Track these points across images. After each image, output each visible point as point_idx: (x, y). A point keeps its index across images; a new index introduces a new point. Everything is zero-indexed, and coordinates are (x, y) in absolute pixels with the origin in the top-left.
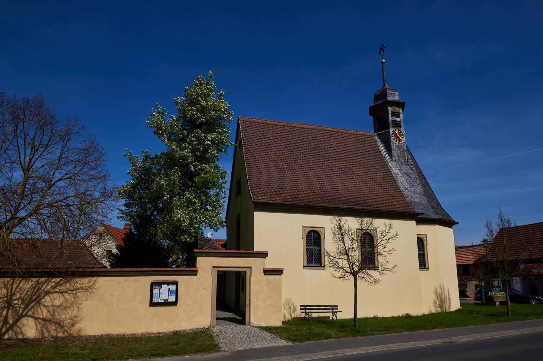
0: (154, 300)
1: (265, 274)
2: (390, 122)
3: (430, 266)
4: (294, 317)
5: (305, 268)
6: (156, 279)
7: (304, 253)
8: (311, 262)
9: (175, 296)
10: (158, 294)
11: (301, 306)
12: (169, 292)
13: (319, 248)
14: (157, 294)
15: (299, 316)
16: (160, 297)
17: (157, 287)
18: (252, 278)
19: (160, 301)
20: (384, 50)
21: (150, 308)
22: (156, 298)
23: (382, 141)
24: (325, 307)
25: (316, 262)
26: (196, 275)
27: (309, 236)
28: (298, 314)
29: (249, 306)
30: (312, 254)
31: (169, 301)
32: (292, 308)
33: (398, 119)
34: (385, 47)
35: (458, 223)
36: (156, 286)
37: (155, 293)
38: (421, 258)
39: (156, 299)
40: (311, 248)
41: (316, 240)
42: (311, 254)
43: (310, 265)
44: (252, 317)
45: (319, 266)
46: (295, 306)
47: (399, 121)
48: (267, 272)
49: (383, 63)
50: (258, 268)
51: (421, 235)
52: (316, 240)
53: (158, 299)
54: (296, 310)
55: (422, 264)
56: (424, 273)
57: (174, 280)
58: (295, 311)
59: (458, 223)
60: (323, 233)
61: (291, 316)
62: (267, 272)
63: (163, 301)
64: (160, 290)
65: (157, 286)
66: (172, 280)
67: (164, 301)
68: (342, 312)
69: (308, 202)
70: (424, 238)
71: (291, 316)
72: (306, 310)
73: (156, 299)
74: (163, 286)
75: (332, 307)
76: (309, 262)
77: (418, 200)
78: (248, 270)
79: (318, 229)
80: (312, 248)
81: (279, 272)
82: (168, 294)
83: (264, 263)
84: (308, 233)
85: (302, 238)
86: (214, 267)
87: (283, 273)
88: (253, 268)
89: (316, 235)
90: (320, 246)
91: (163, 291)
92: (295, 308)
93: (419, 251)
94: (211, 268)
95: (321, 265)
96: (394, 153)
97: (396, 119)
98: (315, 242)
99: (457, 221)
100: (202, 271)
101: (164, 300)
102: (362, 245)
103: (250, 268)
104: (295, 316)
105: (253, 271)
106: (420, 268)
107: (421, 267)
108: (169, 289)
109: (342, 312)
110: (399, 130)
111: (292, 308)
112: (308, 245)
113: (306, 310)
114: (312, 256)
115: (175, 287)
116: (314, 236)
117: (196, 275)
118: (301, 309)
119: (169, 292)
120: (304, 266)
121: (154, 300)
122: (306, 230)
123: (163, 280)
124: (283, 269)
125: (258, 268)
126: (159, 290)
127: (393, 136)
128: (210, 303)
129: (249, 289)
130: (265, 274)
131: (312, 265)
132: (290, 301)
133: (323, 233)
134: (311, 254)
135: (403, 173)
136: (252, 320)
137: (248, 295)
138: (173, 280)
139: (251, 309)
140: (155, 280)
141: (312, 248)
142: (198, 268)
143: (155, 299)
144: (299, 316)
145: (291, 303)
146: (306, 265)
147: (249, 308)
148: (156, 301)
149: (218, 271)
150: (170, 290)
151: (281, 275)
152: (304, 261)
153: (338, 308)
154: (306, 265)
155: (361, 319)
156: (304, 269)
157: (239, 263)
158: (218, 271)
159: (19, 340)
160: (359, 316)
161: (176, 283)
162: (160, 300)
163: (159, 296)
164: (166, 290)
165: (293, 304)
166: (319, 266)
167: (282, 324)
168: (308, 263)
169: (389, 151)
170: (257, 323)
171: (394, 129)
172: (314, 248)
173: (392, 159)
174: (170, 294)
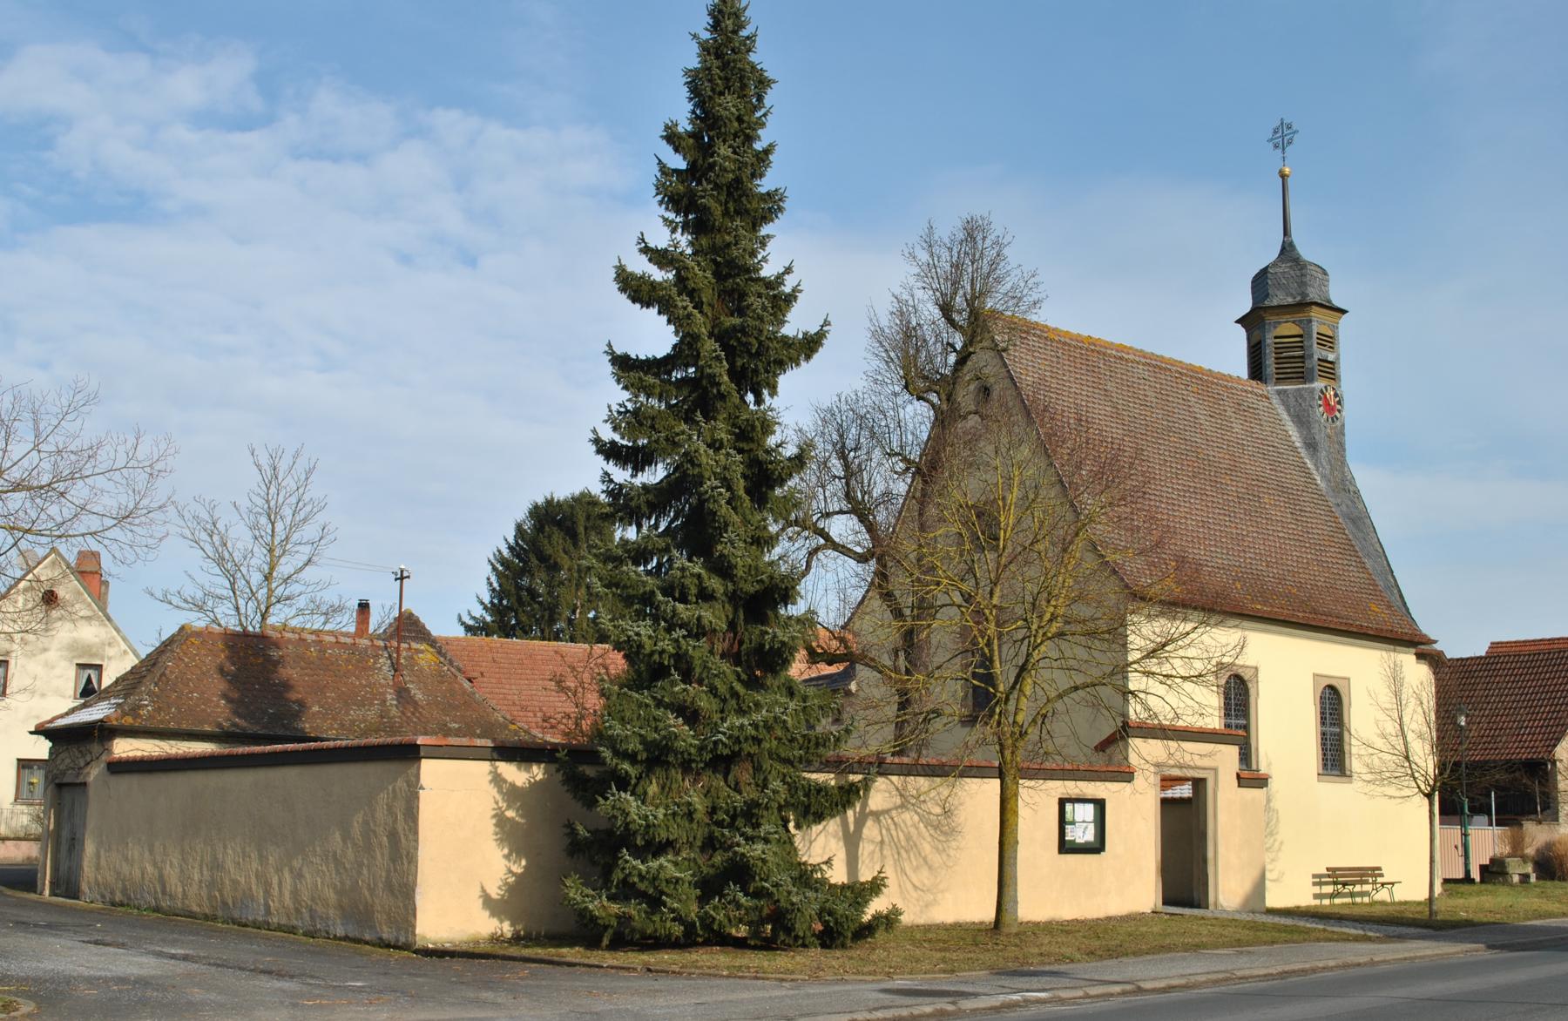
13: (1338, 730)
56: (1334, 789)
154: (1321, 772)
161: (1100, 805)
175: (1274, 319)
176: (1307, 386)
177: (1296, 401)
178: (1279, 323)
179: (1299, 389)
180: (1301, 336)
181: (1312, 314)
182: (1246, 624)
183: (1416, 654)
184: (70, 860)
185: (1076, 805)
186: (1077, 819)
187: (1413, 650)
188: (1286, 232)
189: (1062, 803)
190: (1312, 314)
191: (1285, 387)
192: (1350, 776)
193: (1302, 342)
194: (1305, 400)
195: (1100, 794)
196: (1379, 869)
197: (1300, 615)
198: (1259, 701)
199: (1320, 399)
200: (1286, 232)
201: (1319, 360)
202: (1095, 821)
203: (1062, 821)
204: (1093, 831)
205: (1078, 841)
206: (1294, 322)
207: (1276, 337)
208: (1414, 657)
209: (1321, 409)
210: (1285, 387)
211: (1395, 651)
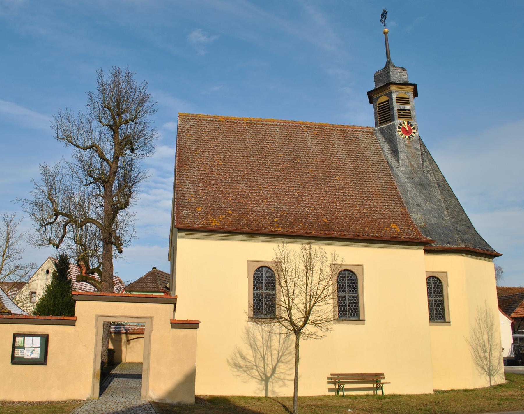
0: (18, 352)
2: (395, 112)
3: (366, 318)
6: (20, 330)
10: (21, 342)
13: (357, 294)
14: (20, 342)
20: (386, 16)
23: (385, 139)
24: (362, 378)
33: (407, 107)
34: (387, 12)
35: (500, 255)
37: (18, 341)
38: (439, 306)
41: (437, 288)
47: (409, 110)
48: (177, 325)
49: (385, 33)
51: (438, 272)
52: (437, 288)
53: (23, 352)
55: (440, 317)
56: (438, 329)
59: (500, 255)
62: (177, 325)
66: (41, 332)
68: (390, 383)
69: (248, 225)
70: (442, 277)
73: (20, 351)
75: (338, 376)
76: (257, 312)
77: (436, 222)
78: (147, 322)
81: (194, 325)
84: (257, 270)
87: (198, 327)
88: (154, 318)
93: (429, 295)
95: (359, 317)
96: (402, 156)
97: (405, 108)
98: (435, 291)
99: (499, 252)
102: (340, 287)
106: (430, 322)
107: (431, 321)
109: (390, 383)
110: (408, 123)
121: (18, 352)
123: (30, 332)
124: (197, 321)
127: (399, 131)
134: (344, 303)
135: (414, 183)
140: (18, 331)
142: (76, 317)
143: (18, 350)
146: (252, 316)
153: (384, 377)
154: (252, 316)
155: (302, 397)
159: (268, 398)
160: (300, 394)
161: (45, 339)
169: (395, 152)
171: (401, 121)
173: (399, 162)
175: (377, 96)
176: (391, 123)
177: (388, 132)
178: (379, 97)
179: (388, 125)
180: (388, 101)
181: (392, 89)
182: (287, 240)
183: (424, 250)
184: (243, 367)
185: (26, 338)
186: (26, 345)
187: (423, 247)
188: (388, 56)
189: (15, 336)
190: (392, 89)
191: (383, 126)
192: (450, 322)
193: (388, 103)
194: (391, 130)
195: (47, 332)
196: (383, 374)
197: (313, 232)
198: (364, 283)
199: (399, 128)
200: (388, 56)
201: (398, 110)
202: (41, 347)
203: (14, 347)
204: (39, 352)
205: (26, 357)
206: (385, 95)
207: (379, 104)
208: (423, 251)
209: (401, 133)
210: (383, 126)
211: (283, 242)
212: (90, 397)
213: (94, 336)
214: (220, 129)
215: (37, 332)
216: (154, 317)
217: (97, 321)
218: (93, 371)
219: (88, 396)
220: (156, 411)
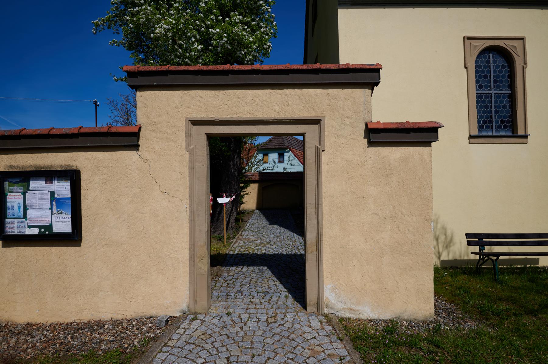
0: (12, 225)
1: (371, 144)
4: (446, 259)
5: (473, 140)
6: (13, 163)
7: (470, 104)
8: (487, 127)
9: (70, 216)
10: (19, 207)
11: (468, 236)
12: (54, 203)
14: (16, 208)
15: (460, 256)
16: (28, 217)
17: (16, 188)
18: (324, 157)
19: (28, 231)
21: (3, 248)
22: (16, 220)
25: (500, 127)
26: (135, 147)
27: (482, 62)
28: (458, 253)
29: (315, 248)
30: (491, 106)
31: (57, 229)
32: (442, 238)
36: (12, 184)
37: (13, 207)
39: (16, 225)
40: (487, 92)
42: (487, 107)
43: (484, 134)
44: (329, 286)
45: (510, 134)
46: (449, 233)
50: (347, 121)
53: (23, 225)
54: (451, 244)
57: (69, 166)
58: (450, 247)
60: (520, 51)
61: (439, 258)
63: (36, 231)
64: (24, 194)
65: (17, 183)
66: (61, 166)
67: (40, 230)
71: (439, 258)
72: (482, 247)
73: (16, 225)
74: (34, 184)
79: (507, 42)
80: (490, 92)
82: (51, 209)
83: (368, 105)
85: (466, 68)
86: (195, 123)
87: (436, 139)
88: (327, 123)
89: (501, 61)
90: (512, 86)
91: (34, 200)
92: (449, 239)
94: (182, 125)
100: (155, 135)
101: (40, 227)
103: (317, 122)
104: (451, 258)
105: (326, 133)
108: (53, 193)
111: (442, 238)
112: (479, 87)
113: (482, 247)
114: (491, 112)
115: (69, 187)
116: (494, 62)
117: (135, 147)
118: (469, 243)
119: (54, 203)
120: (471, 137)
121: (12, 225)
122: (476, 46)
123: (36, 167)
125: (347, 121)
126: (22, 196)
128: (186, 239)
129: (523, 127)
130: (371, 144)
131: (490, 134)
132: (437, 223)
133: (520, 53)
136: (328, 295)
137: (314, 213)
138: (65, 166)
139: (322, 261)
140: (11, 166)
141: (490, 92)
143: (13, 223)
144: (460, 256)
145: (439, 226)
146: (475, 132)
147: (315, 254)
148: (16, 231)
149: (210, 138)
150: (56, 196)
151: (428, 144)
152: (471, 123)
154: (475, 132)
156: (470, 143)
157: (277, 108)
158: (210, 138)
162: (30, 227)
163: (25, 216)
164: (42, 198)
165: (444, 229)
166: (510, 134)
167: (433, 311)
168: (481, 128)
170: (345, 304)
172: (495, 92)
174: (55, 210)
212: (186, 309)
213: (186, 170)
214: (92, 356)
215: (52, 166)
216: (326, 119)
217: (189, 135)
218: (190, 249)
219: (184, 307)
220: (413, 316)
